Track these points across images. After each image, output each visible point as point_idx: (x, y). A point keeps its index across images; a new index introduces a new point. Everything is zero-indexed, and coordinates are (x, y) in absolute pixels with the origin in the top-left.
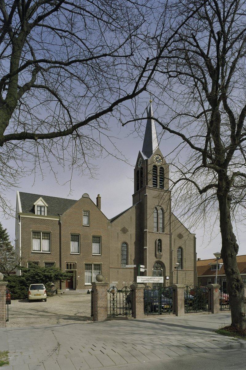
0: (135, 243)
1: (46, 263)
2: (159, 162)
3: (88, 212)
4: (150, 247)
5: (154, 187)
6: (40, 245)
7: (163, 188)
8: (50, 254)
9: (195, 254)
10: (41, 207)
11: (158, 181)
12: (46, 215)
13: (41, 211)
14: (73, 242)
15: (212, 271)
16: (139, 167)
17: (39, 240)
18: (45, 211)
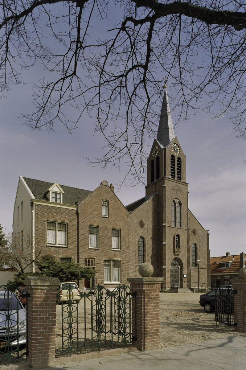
0: (152, 238)
1: (62, 259)
2: (176, 151)
3: (108, 201)
4: (168, 242)
5: (173, 178)
6: (55, 238)
7: (181, 180)
8: (67, 248)
9: (208, 251)
10: (56, 194)
11: (176, 173)
12: (62, 203)
13: (56, 198)
14: (91, 235)
15: (220, 270)
16: (154, 156)
17: (54, 232)
18: (60, 199)
